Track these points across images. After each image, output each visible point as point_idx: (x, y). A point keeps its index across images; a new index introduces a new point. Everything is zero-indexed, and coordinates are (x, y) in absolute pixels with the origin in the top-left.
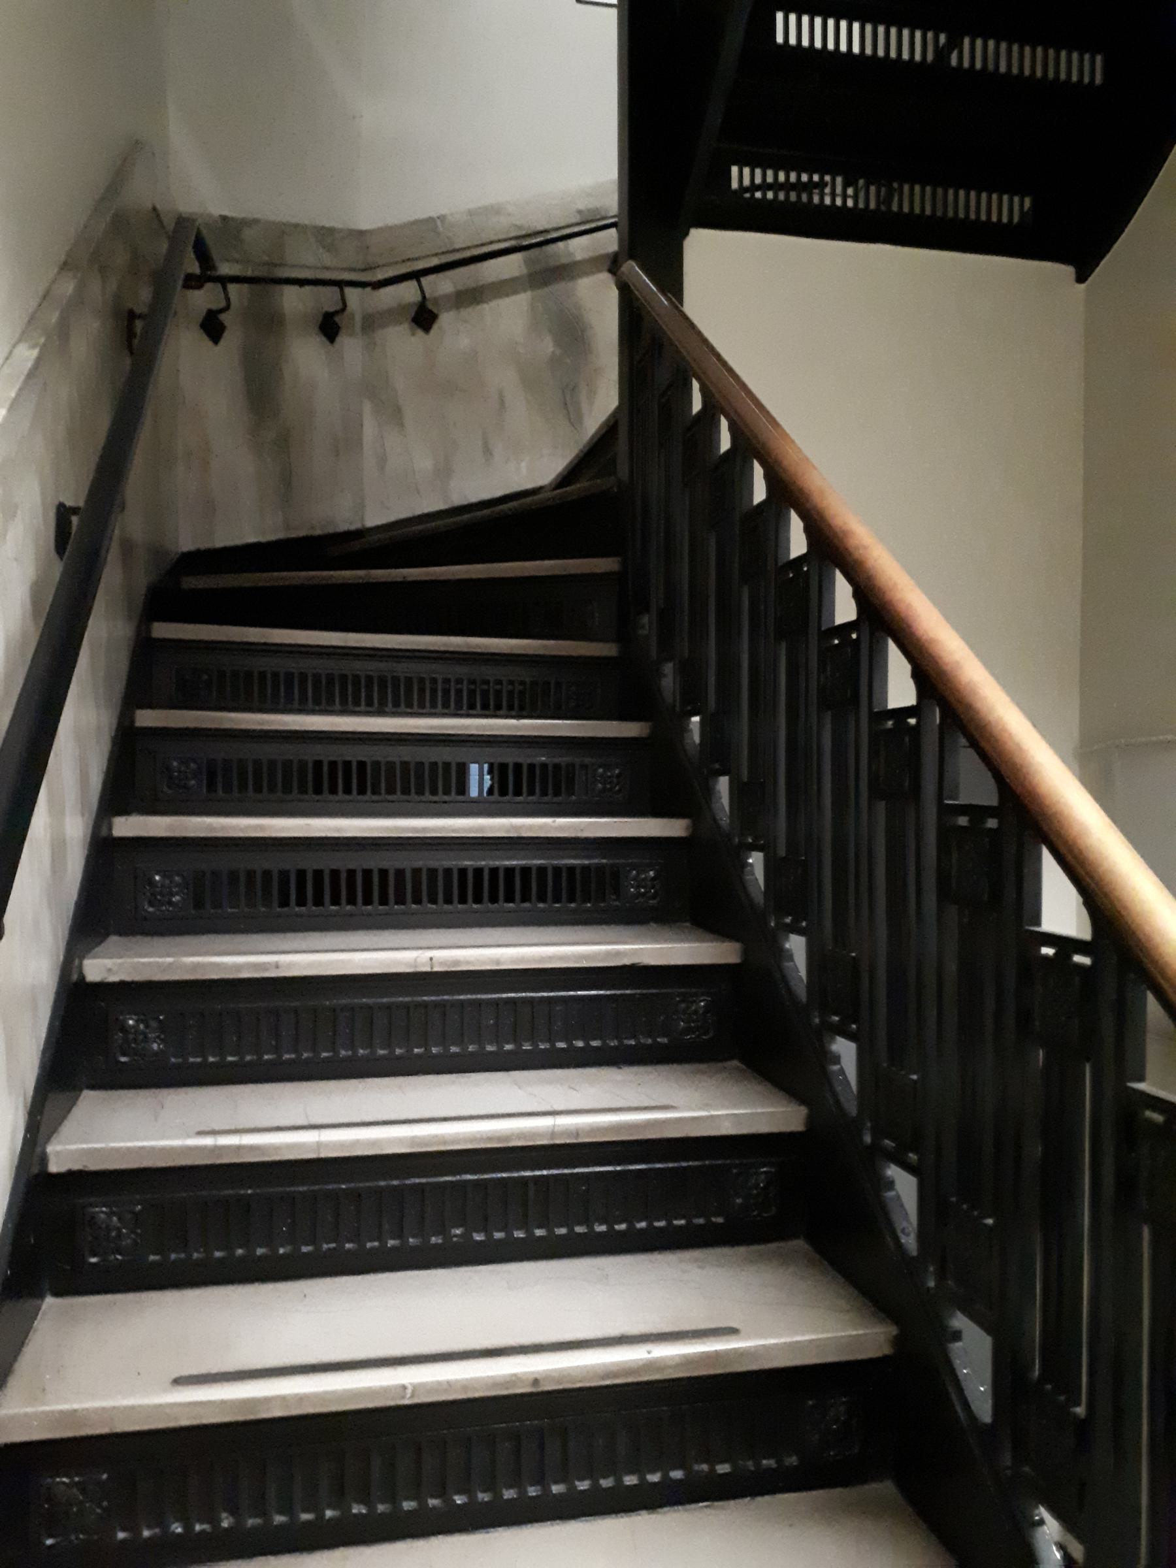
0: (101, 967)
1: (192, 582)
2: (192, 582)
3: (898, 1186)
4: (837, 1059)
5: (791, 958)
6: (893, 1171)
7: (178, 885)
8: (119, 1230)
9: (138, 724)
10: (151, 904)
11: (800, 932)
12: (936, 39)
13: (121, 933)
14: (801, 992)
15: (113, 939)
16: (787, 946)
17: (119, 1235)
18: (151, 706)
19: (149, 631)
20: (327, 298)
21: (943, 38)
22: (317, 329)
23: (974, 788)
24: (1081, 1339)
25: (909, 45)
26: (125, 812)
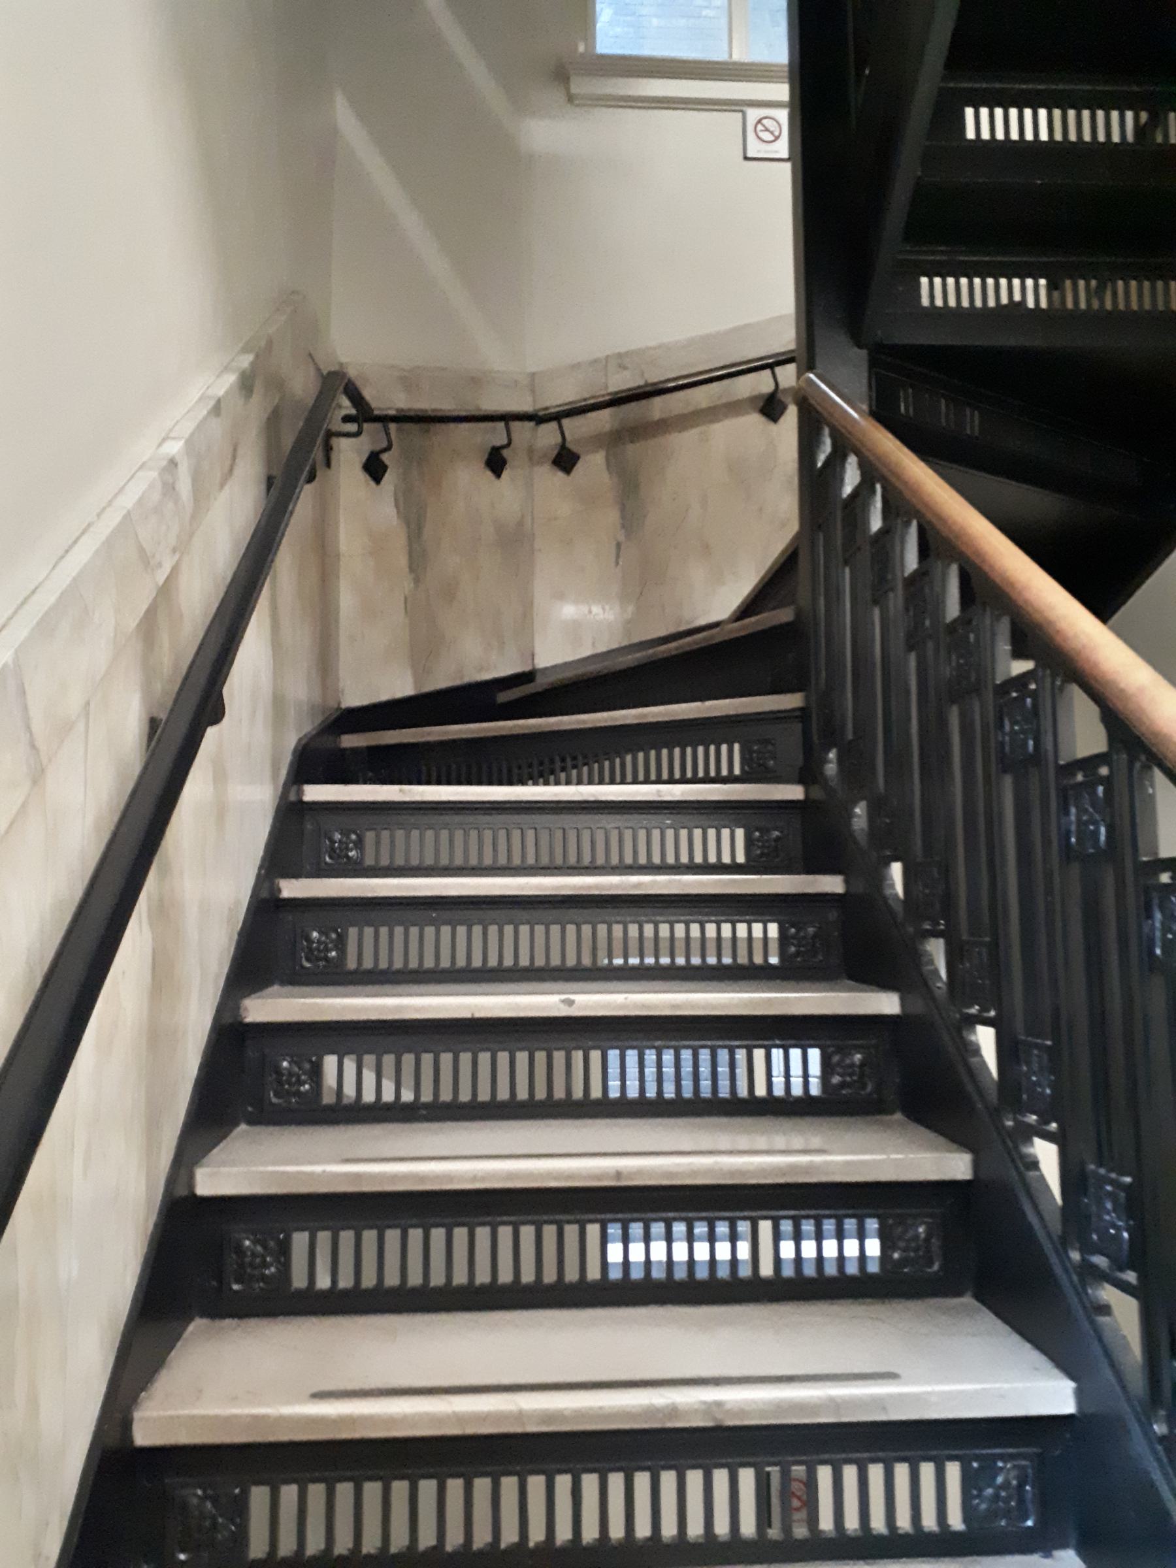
0: (223, 1176)
1: (350, 741)
2: (350, 741)
3: (1116, 1310)
4: (1034, 1165)
5: (931, 962)
6: (1108, 1294)
7: (332, 941)
8: (214, 1518)
9: (249, 1019)
10: (308, 960)
11: (987, 1022)
12: (1136, 118)
13: (283, 983)
14: (862, 839)
15: (276, 988)
16: (973, 1038)
17: (215, 1525)
18: (296, 876)
19: (300, 793)
20: (496, 435)
21: (1144, 116)
22: (481, 465)
23: (1085, 736)
24: (875, 711)
25: (1117, 126)
26: (296, 874)
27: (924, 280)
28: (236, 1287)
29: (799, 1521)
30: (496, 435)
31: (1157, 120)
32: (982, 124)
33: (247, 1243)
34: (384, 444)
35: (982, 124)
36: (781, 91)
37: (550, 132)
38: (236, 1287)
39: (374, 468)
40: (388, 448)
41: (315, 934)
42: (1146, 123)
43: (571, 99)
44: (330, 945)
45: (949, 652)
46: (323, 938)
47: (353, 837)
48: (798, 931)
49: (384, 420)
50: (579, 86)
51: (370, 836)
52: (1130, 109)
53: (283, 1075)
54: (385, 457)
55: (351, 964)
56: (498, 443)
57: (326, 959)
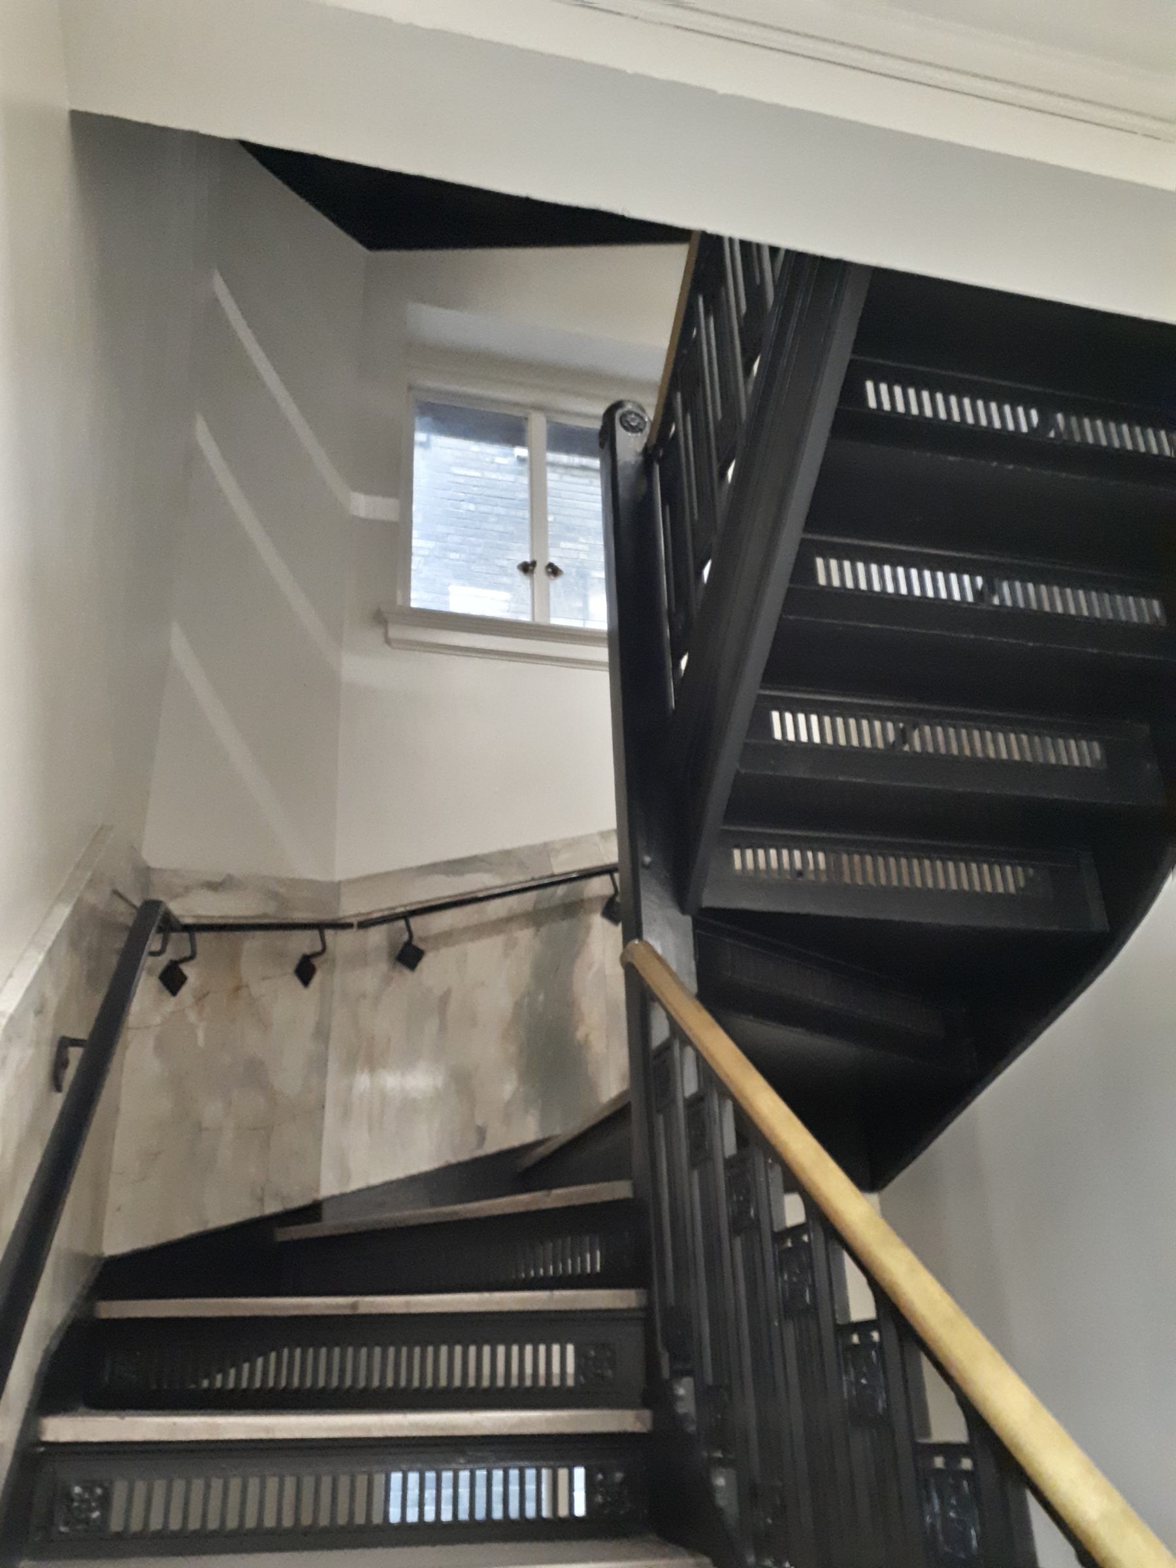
20: (304, 943)
27: (737, 853)
28: (63, 1529)
29: (839, 865)
30: (304, 943)
31: (992, 587)
32: (791, 727)
33: (77, 1490)
34: (188, 953)
35: (791, 727)
36: (602, 653)
37: (366, 667)
38: (63, 1529)
39: (172, 980)
40: (192, 957)
41: (77, 1490)
42: (983, 587)
43: (388, 641)
44: (93, 1504)
45: (758, 1220)
46: (87, 1496)
47: (99, 1491)
48: (605, 1477)
49: (188, 928)
50: (395, 632)
51: (120, 1491)
52: (994, 400)
53: (72, 1500)
54: (186, 969)
55: (116, 1525)
56: (307, 950)
57: (87, 1521)
